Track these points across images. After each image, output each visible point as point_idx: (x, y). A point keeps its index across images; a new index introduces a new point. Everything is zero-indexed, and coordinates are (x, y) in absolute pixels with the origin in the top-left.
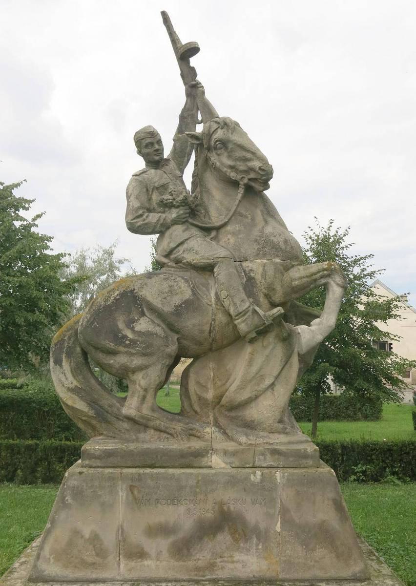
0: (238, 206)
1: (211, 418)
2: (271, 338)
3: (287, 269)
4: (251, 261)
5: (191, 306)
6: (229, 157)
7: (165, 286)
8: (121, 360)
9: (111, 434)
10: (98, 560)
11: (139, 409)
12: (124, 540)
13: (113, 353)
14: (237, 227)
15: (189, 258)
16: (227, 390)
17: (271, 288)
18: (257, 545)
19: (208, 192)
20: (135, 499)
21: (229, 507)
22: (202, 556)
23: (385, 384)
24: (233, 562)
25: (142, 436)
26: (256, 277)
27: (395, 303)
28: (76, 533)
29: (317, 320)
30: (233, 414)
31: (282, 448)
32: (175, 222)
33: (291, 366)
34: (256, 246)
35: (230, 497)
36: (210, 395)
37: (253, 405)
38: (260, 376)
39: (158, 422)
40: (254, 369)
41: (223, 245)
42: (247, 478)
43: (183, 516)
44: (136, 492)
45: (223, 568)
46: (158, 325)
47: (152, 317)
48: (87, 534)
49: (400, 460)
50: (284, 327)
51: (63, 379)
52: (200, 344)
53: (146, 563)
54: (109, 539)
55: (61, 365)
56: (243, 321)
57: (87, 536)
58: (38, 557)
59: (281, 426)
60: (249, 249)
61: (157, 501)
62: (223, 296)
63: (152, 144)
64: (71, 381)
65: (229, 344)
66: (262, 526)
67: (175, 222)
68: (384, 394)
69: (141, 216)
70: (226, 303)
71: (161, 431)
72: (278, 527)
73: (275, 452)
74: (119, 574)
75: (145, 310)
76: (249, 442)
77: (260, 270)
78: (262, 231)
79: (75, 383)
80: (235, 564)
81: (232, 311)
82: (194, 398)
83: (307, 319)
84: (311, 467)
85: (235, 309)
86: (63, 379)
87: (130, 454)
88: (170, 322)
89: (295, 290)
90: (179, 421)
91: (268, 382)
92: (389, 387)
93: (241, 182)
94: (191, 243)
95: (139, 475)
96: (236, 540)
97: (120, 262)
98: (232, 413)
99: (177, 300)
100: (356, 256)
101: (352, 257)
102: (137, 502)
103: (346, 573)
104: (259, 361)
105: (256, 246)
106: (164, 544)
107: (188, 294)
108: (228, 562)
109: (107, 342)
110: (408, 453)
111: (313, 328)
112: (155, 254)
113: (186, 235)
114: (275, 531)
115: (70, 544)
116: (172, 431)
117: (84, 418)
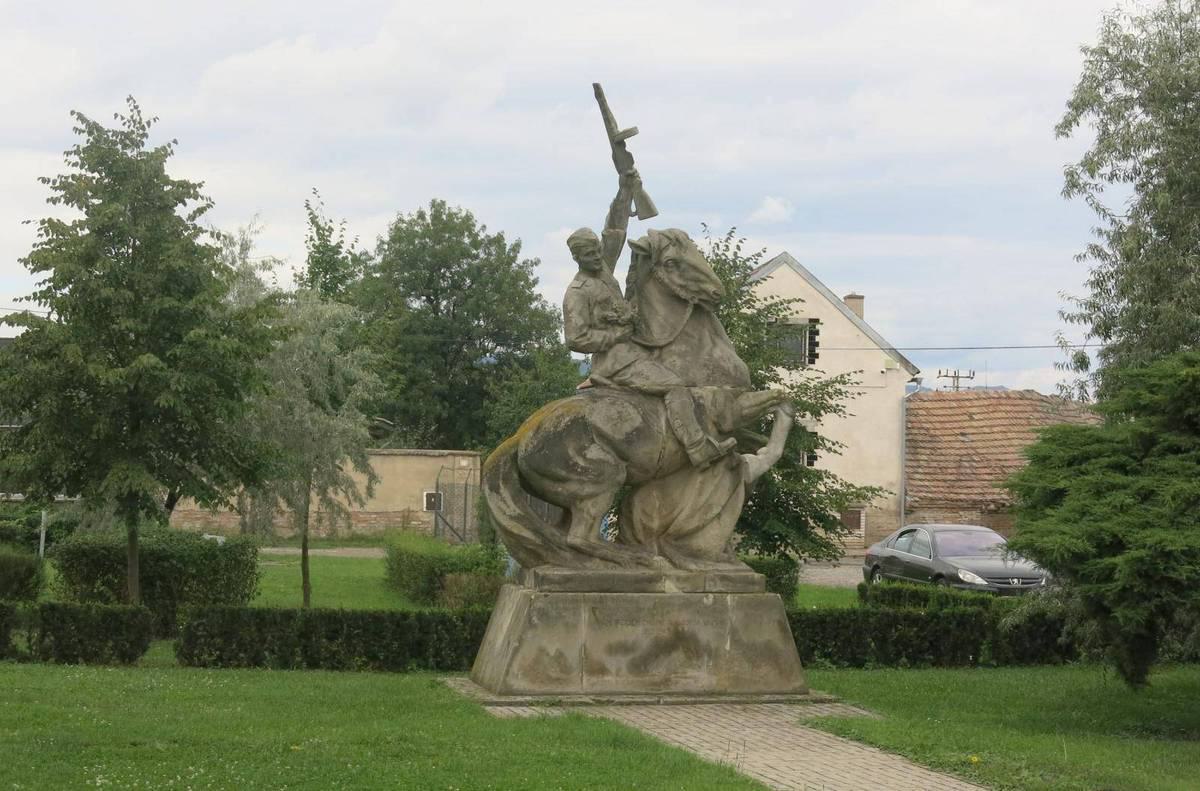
0: (686, 325)
1: (656, 548)
2: (721, 467)
3: (737, 395)
4: (701, 388)
5: (641, 434)
6: (681, 276)
7: (613, 411)
8: (573, 487)
9: (558, 563)
10: (563, 676)
11: (586, 538)
12: (587, 658)
13: (563, 480)
14: (683, 348)
15: (638, 382)
16: (673, 520)
17: (721, 416)
18: (708, 662)
19: (649, 304)
20: (597, 620)
21: (683, 629)
22: (658, 672)
23: (813, 528)
24: (686, 678)
25: (588, 564)
26: (706, 404)
27: (838, 386)
28: (542, 650)
29: (764, 449)
30: (680, 543)
31: (732, 574)
32: (619, 341)
33: (738, 494)
34: (705, 372)
35: (683, 617)
36: (655, 524)
37: (700, 534)
38: (708, 506)
39: (605, 551)
40: (703, 499)
41: (668, 366)
42: (700, 601)
43: (640, 635)
44: (597, 613)
45: (677, 683)
46: (608, 453)
47: (935, 514)
48: (552, 652)
49: (836, 637)
50: (734, 457)
51: (504, 507)
52: (647, 471)
53: (606, 678)
54: (573, 656)
55: (498, 492)
56: (696, 452)
57: (552, 653)
58: (507, 672)
59: (726, 555)
60: (699, 374)
61: (617, 622)
62: (676, 425)
63: (593, 253)
64: (513, 509)
65: (677, 471)
66: (713, 645)
67: (619, 341)
68: (811, 544)
69: (585, 335)
70: (680, 432)
71: (607, 560)
72: (728, 647)
73: (724, 578)
74: (582, 688)
75: (595, 437)
76: (699, 569)
77: (711, 397)
78: (711, 355)
79: (518, 511)
80: (688, 680)
81: (686, 440)
82: (638, 526)
83: (752, 446)
84: (758, 592)
85: (689, 438)
86: (504, 507)
87: (587, 579)
88: (620, 450)
89: (743, 418)
90: (627, 550)
91: (716, 511)
92: (820, 532)
93: (691, 302)
94: (640, 367)
95: (601, 597)
96: (690, 658)
97: (265, 266)
98: (677, 542)
99: (627, 428)
100: (772, 297)
101: (765, 299)
102: (599, 622)
103: (789, 688)
104: (709, 488)
105: (705, 372)
106: (623, 661)
107: (638, 421)
108: (681, 677)
109: (558, 470)
110: (847, 627)
111: (760, 457)
112: (316, 238)
113: (631, 357)
114: (725, 650)
115: (537, 661)
116: (620, 560)
117: (531, 547)
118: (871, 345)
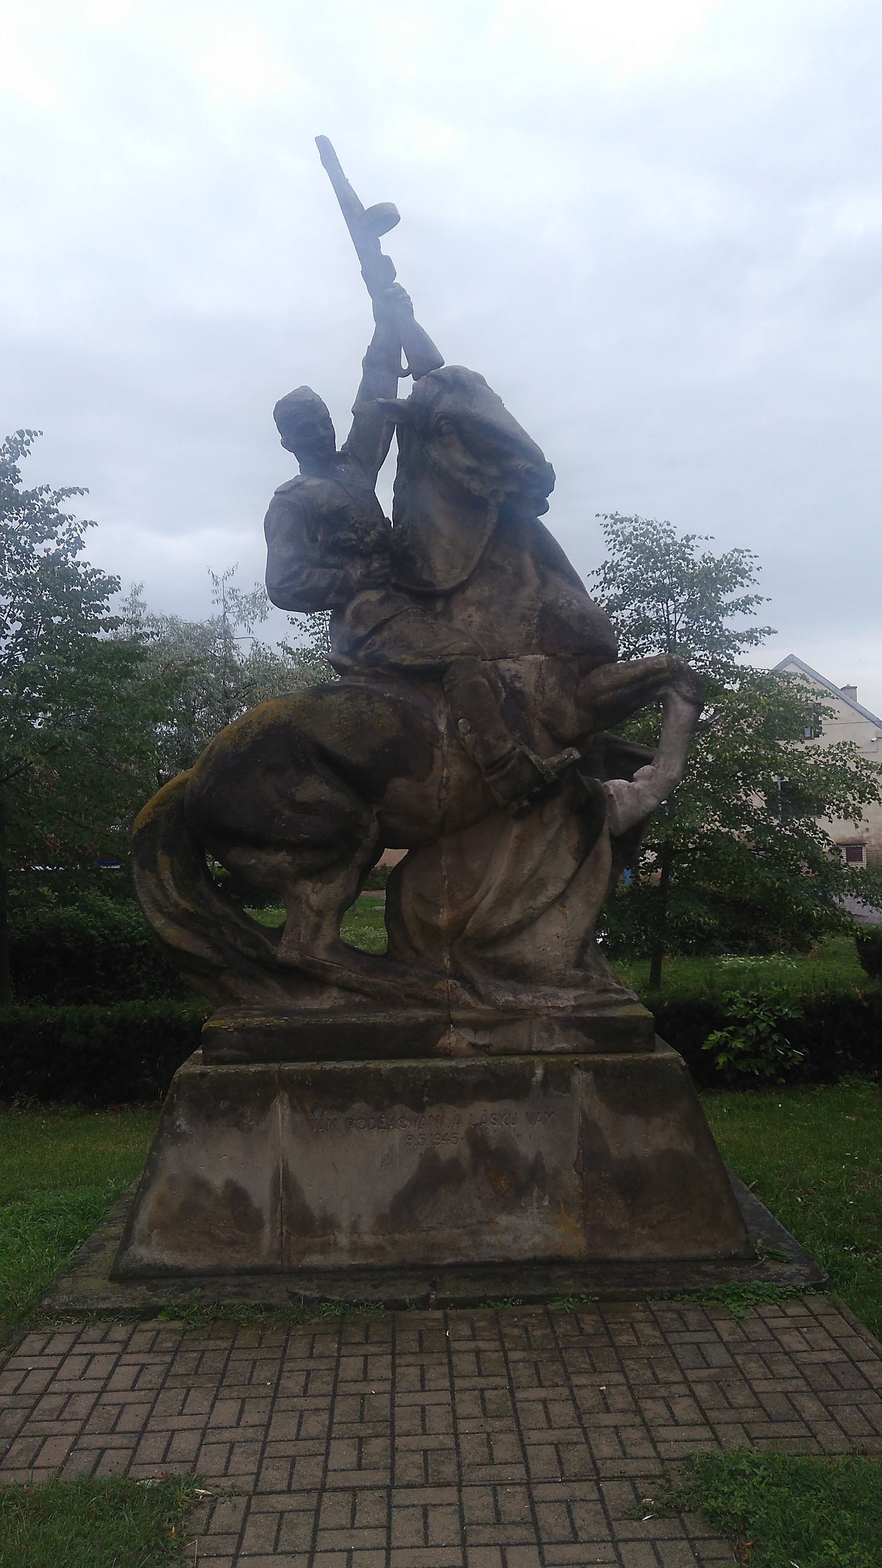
2: (555, 810)
16: (475, 908)
18: (540, 1199)
29: (647, 768)
40: (527, 868)
77: (533, 677)
91: (553, 890)
104: (538, 849)
118: (865, 720)
